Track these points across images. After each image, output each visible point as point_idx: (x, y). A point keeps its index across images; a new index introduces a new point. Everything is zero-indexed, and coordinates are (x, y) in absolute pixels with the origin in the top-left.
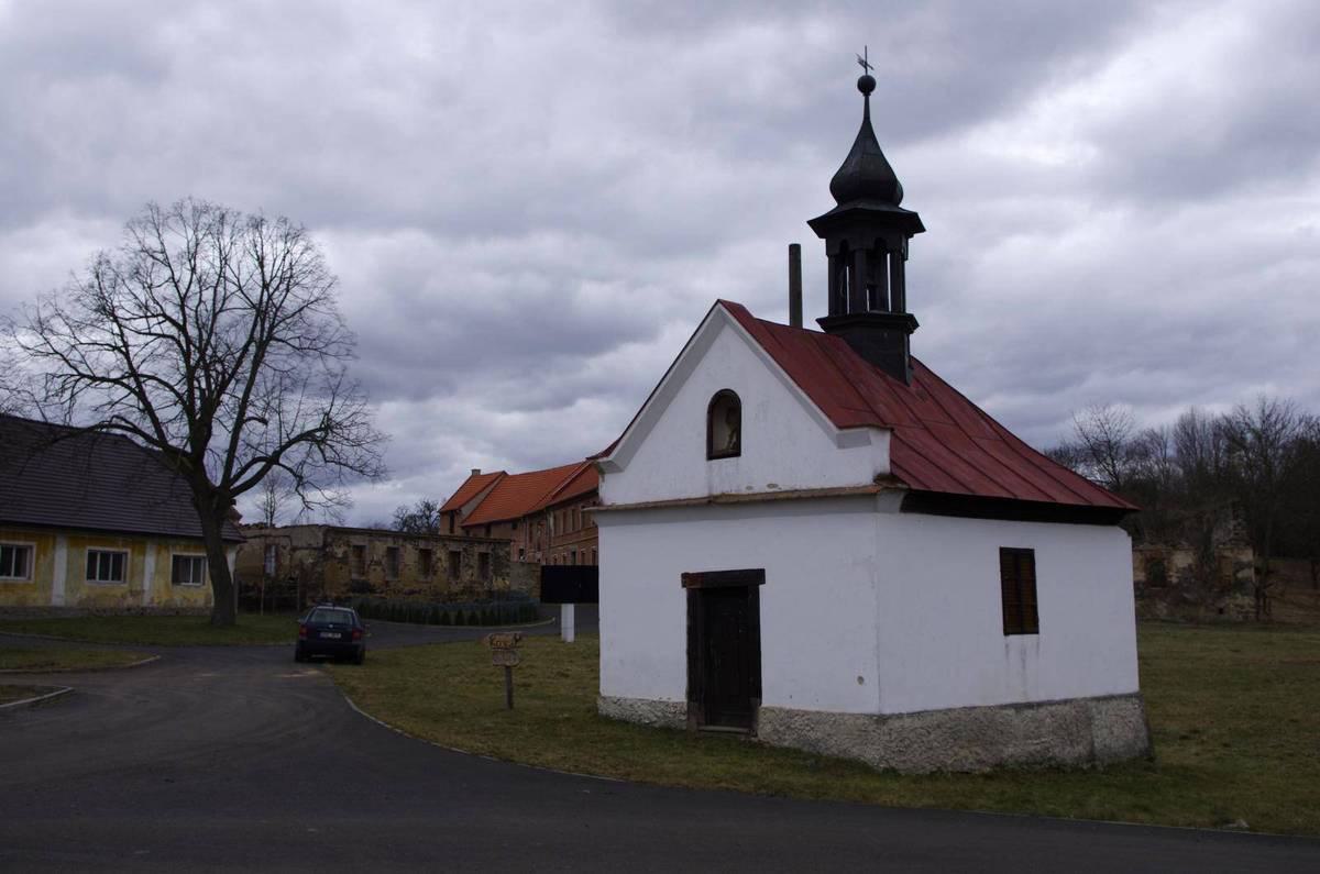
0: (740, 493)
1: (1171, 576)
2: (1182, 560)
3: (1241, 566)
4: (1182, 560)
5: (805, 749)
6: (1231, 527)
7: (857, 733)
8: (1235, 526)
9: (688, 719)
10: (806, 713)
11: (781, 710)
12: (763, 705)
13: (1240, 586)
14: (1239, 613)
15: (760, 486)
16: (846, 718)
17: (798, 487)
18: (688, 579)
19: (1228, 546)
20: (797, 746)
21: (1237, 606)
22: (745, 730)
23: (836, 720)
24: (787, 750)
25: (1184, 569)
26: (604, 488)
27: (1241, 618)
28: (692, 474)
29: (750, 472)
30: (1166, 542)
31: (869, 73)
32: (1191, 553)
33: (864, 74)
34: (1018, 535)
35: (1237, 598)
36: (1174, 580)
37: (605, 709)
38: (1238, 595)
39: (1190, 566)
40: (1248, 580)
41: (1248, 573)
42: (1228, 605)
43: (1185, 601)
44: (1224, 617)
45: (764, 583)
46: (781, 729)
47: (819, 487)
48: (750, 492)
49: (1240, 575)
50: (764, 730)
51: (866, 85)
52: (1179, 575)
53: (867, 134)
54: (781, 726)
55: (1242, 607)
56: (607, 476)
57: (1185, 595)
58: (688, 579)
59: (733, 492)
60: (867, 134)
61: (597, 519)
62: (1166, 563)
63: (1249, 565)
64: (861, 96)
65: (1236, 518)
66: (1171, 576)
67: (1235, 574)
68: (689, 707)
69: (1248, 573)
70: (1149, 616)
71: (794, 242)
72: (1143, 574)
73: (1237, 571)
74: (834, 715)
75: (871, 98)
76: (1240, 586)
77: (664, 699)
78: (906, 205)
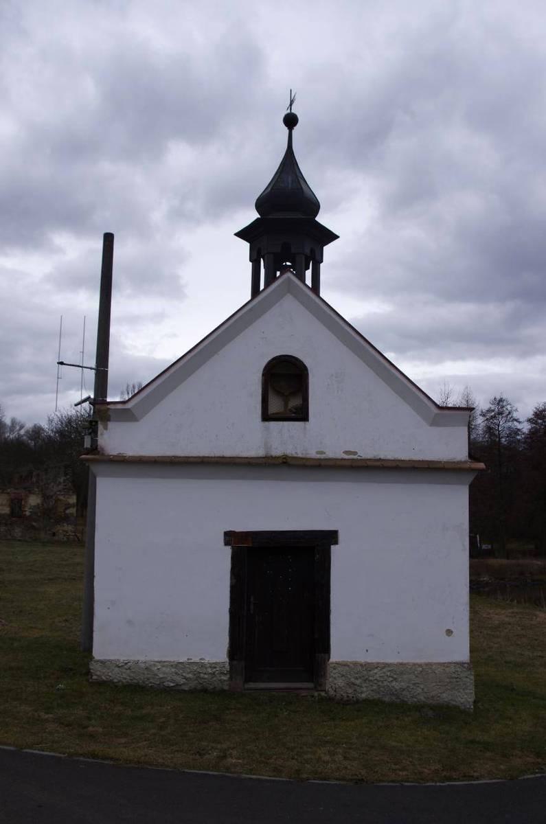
0: (308, 456)
1: (25, 511)
2: (34, 500)
3: (68, 506)
4: (34, 500)
5: (387, 699)
6: (62, 480)
7: (448, 680)
8: (64, 480)
9: (231, 678)
10: (387, 665)
11: (355, 664)
12: (331, 660)
13: (66, 519)
14: (64, 536)
15: (334, 450)
16: (434, 667)
17: (382, 457)
18: (231, 538)
19: (62, 493)
20: (376, 697)
21: (64, 531)
22: (310, 685)
23: (425, 670)
24: (366, 701)
25: (34, 506)
26: (106, 436)
27: (65, 539)
28: (252, 435)
29: (323, 433)
30: (25, 488)
31: (293, 111)
32: (40, 496)
33: (289, 111)
34: (287, 438)
35: (64, 526)
36: (28, 513)
37: (98, 671)
38: (65, 524)
39: (38, 504)
40: (72, 514)
41: (72, 511)
42: (59, 530)
43: (33, 527)
44: (56, 538)
45: (336, 543)
46: (358, 682)
47: (407, 459)
48: (322, 456)
49: (68, 511)
50: (335, 683)
51: (291, 121)
52: (31, 510)
53: (289, 162)
54: (357, 679)
55: (67, 532)
56: (110, 425)
57: (34, 524)
58: (231, 538)
59: (300, 455)
60: (289, 162)
61: (94, 468)
62: (23, 503)
63: (73, 506)
64: (286, 130)
65: (66, 474)
66: (25, 511)
67: (64, 512)
68: (231, 668)
69: (72, 511)
70: (9, 537)
71: (108, 231)
72: (8, 509)
73: (66, 509)
74: (420, 665)
75: (293, 131)
76: (66, 519)
77: (197, 660)
78: (321, 219)
